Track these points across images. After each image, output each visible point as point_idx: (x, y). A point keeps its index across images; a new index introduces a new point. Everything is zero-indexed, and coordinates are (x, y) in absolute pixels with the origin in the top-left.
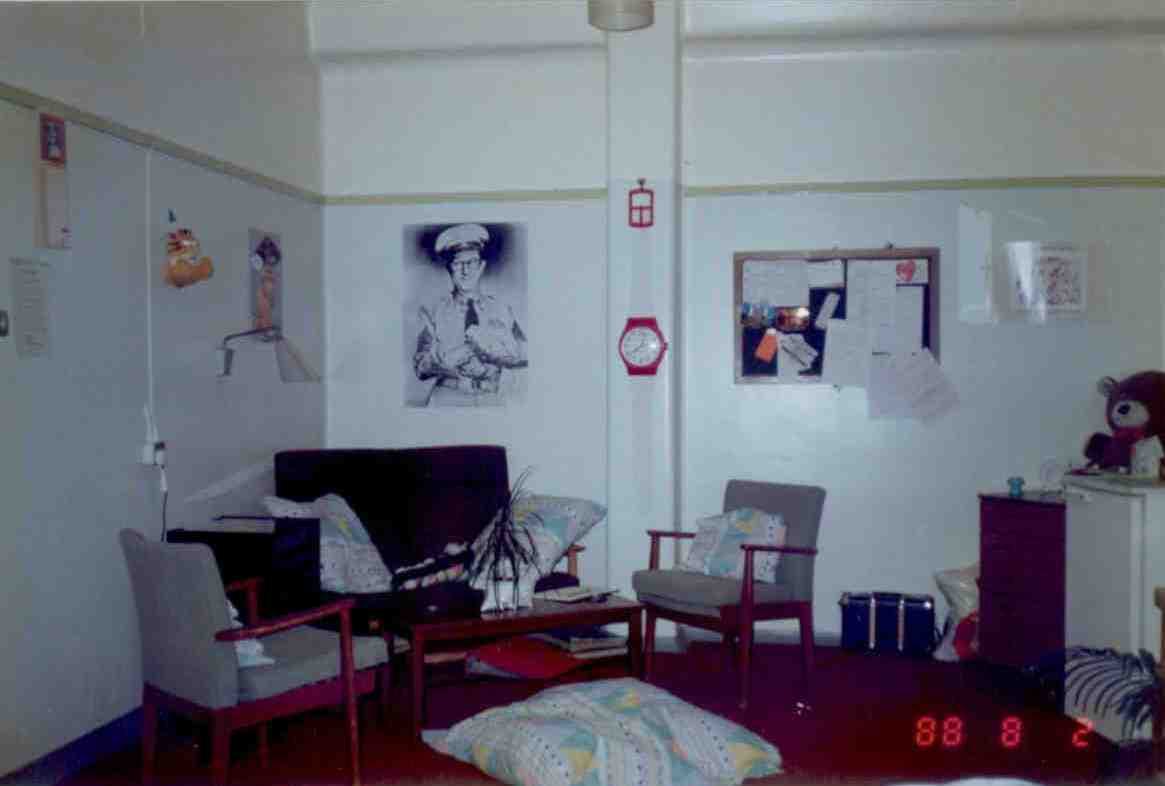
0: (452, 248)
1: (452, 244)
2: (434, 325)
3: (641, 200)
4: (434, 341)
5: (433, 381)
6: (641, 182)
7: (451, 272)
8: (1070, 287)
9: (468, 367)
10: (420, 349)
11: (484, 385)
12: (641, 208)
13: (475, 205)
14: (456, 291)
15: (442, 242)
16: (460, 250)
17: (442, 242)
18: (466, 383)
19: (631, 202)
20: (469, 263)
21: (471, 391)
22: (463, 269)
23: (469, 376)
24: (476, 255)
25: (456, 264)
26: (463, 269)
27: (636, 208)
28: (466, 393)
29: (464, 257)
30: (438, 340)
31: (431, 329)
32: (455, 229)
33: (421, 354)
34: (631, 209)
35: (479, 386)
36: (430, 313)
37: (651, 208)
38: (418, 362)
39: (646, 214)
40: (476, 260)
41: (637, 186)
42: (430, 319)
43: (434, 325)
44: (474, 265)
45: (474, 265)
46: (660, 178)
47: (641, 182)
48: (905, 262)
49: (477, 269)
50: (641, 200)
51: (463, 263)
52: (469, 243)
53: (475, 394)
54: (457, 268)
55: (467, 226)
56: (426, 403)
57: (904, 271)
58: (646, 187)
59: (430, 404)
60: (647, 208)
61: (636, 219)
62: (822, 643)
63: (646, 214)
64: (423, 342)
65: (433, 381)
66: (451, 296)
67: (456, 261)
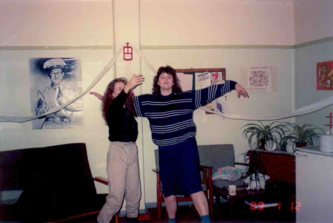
0: (50, 67)
1: (50, 66)
2: (44, 97)
3: (128, 57)
4: (44, 104)
5: (44, 119)
6: (128, 44)
7: (50, 77)
8: (265, 80)
9: (58, 113)
10: (38, 107)
11: (65, 120)
12: (128, 53)
13: (56, 51)
14: (53, 84)
15: (46, 65)
16: (54, 68)
17: (46, 65)
18: (58, 119)
19: (132, 56)
20: (58, 73)
21: (60, 122)
22: (55, 76)
23: (59, 117)
24: (60, 70)
25: (52, 74)
26: (55, 76)
27: (130, 53)
28: (58, 123)
29: (55, 71)
30: (45, 103)
31: (43, 100)
32: (51, 60)
33: (38, 109)
34: (132, 53)
35: (63, 121)
36: (42, 92)
37: (124, 53)
38: (37, 112)
39: (126, 51)
40: (60, 72)
41: (126, 45)
42: (42, 95)
43: (44, 97)
44: (60, 74)
45: (60, 74)
46: (134, 44)
47: (128, 44)
48: (215, 73)
49: (61, 75)
50: (128, 57)
51: (55, 73)
52: (57, 65)
53: (62, 123)
54: (53, 75)
55: (55, 57)
56: (41, 128)
57: (215, 76)
58: (129, 45)
59: (43, 128)
60: (126, 53)
61: (130, 50)
62: (158, 167)
63: (126, 51)
64: (40, 104)
65: (44, 119)
66: (51, 86)
67: (52, 72)
